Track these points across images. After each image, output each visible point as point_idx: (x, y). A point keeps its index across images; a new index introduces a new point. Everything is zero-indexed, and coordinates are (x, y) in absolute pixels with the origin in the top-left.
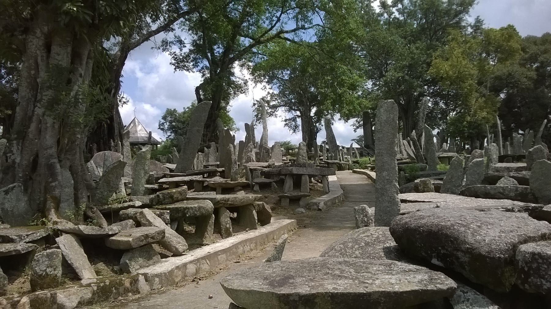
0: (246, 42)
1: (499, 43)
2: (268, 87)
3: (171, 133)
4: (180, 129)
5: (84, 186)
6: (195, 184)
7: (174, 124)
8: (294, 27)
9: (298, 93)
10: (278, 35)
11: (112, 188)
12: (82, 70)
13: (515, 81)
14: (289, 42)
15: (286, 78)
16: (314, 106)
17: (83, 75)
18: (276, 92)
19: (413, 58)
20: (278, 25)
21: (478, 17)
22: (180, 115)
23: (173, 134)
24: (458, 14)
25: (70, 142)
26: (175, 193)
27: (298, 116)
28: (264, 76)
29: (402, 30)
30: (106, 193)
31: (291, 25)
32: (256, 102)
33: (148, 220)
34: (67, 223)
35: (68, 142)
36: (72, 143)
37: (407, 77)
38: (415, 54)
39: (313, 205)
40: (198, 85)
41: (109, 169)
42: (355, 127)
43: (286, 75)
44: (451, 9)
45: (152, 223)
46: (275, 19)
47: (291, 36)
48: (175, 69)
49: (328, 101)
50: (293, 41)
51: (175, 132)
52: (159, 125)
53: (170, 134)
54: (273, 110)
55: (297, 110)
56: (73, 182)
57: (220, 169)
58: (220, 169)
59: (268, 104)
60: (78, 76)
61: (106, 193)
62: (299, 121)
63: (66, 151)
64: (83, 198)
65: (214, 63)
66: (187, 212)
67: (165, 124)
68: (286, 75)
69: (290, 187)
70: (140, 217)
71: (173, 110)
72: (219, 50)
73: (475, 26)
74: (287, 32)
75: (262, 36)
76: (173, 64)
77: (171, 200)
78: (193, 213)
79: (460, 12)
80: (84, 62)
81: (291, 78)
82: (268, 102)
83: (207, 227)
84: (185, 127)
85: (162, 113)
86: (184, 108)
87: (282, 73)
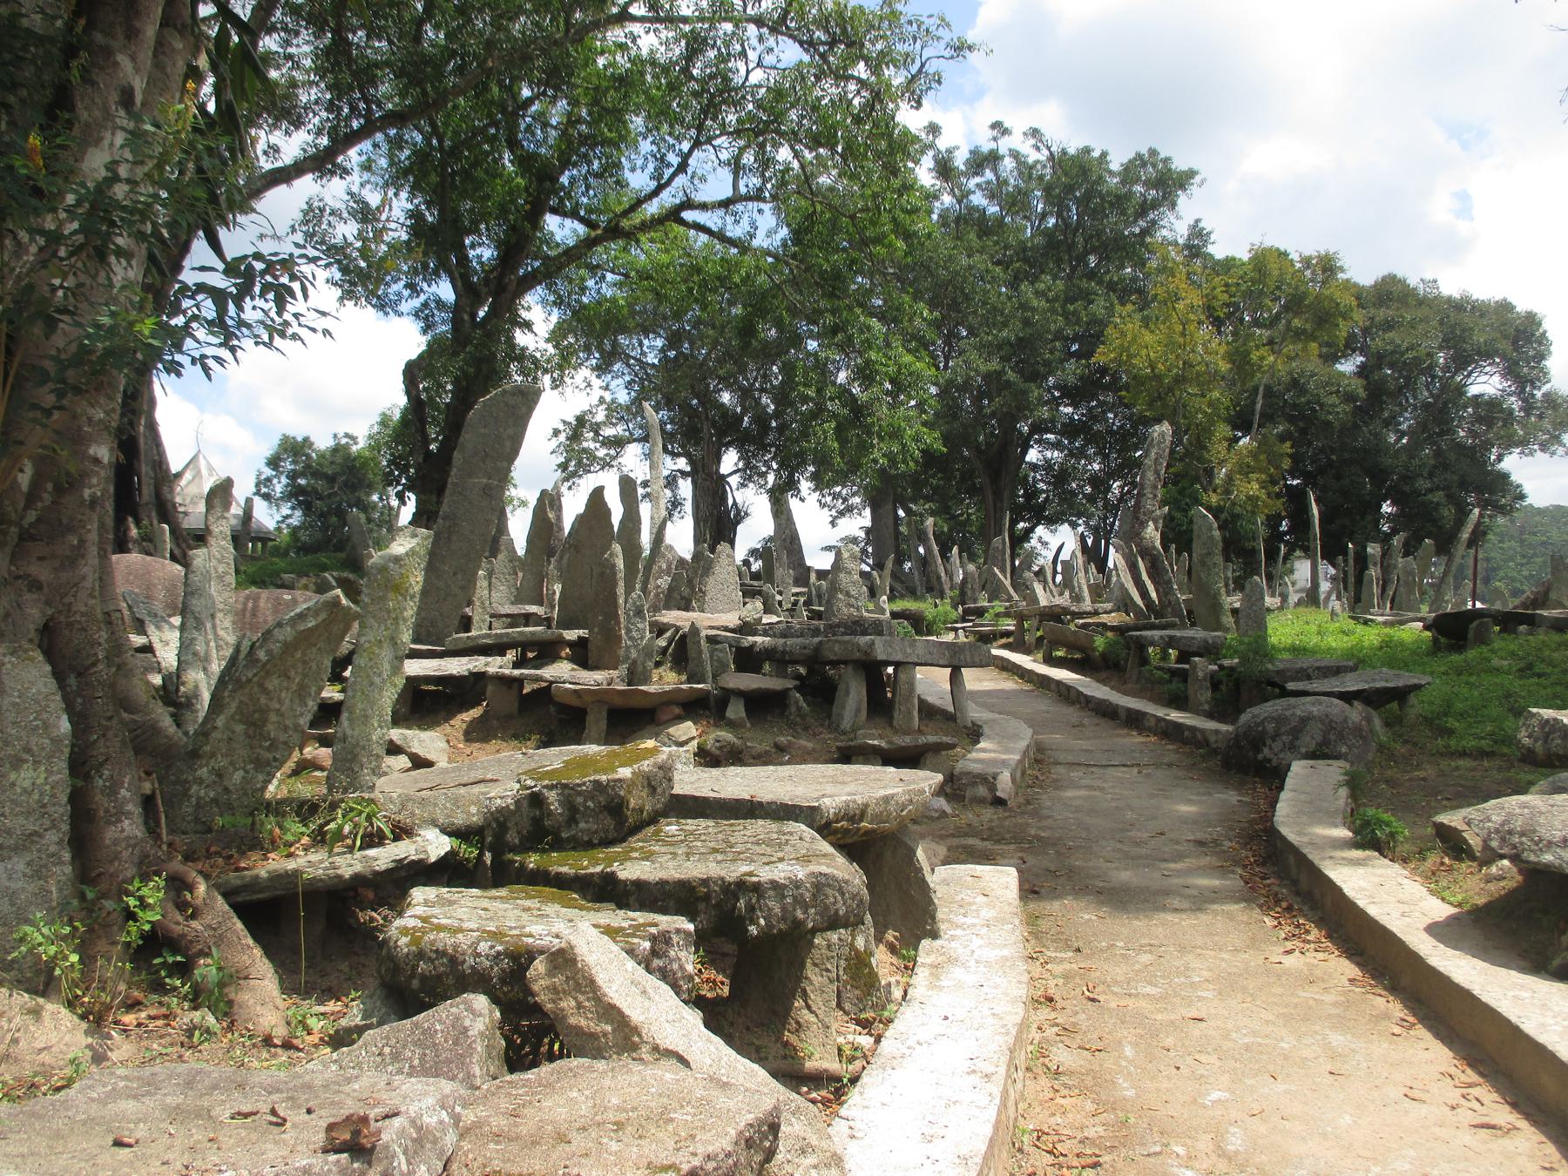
0: (561, 230)
1: (1297, 288)
2: (596, 383)
3: (293, 508)
4: (321, 498)
5: (123, 743)
6: (490, 689)
7: (302, 481)
8: (727, 192)
9: (685, 407)
10: (674, 214)
11: (268, 749)
12: (137, 70)
13: (1308, 402)
14: (704, 238)
15: (652, 359)
16: (728, 445)
17: (139, 99)
18: (623, 397)
19: (1027, 323)
20: (681, 180)
21: (1198, 221)
22: (322, 455)
23: (298, 513)
24: (1144, 208)
25: (50, 486)
26: (631, 784)
27: (684, 474)
28: (587, 349)
29: (996, 243)
30: (240, 773)
31: (718, 186)
32: (561, 427)
33: (611, 1012)
34: (36, 1013)
35: (36, 484)
36: (59, 490)
37: (1011, 375)
38: (1033, 310)
39: (974, 784)
40: (414, 356)
41: (276, 647)
42: (834, 513)
43: (652, 349)
44: (1130, 194)
45: (636, 1030)
46: (674, 159)
47: (716, 219)
48: (341, 299)
49: (826, 426)
50: (720, 236)
51: (307, 507)
52: (258, 485)
53: (289, 512)
54: (612, 452)
55: (678, 455)
56: (65, 725)
57: (571, 635)
58: (571, 635)
59: (597, 434)
60: (114, 97)
61: (240, 773)
62: (686, 488)
63: (21, 538)
64: (120, 814)
65: (468, 292)
66: (751, 909)
67: (275, 481)
68: (652, 349)
69: (858, 711)
70: (554, 989)
71: (300, 439)
72: (483, 252)
73: (1188, 246)
74: (704, 207)
75: (626, 213)
76: (336, 284)
77: (609, 822)
78: (784, 918)
79: (1155, 205)
80: (150, 31)
81: (665, 359)
82: (596, 428)
83: (802, 966)
84: (335, 494)
85: (268, 448)
86: (335, 436)
87: (641, 345)
